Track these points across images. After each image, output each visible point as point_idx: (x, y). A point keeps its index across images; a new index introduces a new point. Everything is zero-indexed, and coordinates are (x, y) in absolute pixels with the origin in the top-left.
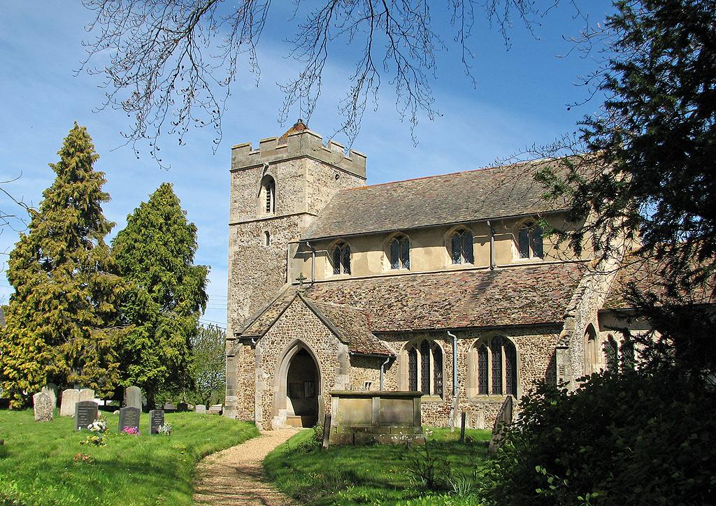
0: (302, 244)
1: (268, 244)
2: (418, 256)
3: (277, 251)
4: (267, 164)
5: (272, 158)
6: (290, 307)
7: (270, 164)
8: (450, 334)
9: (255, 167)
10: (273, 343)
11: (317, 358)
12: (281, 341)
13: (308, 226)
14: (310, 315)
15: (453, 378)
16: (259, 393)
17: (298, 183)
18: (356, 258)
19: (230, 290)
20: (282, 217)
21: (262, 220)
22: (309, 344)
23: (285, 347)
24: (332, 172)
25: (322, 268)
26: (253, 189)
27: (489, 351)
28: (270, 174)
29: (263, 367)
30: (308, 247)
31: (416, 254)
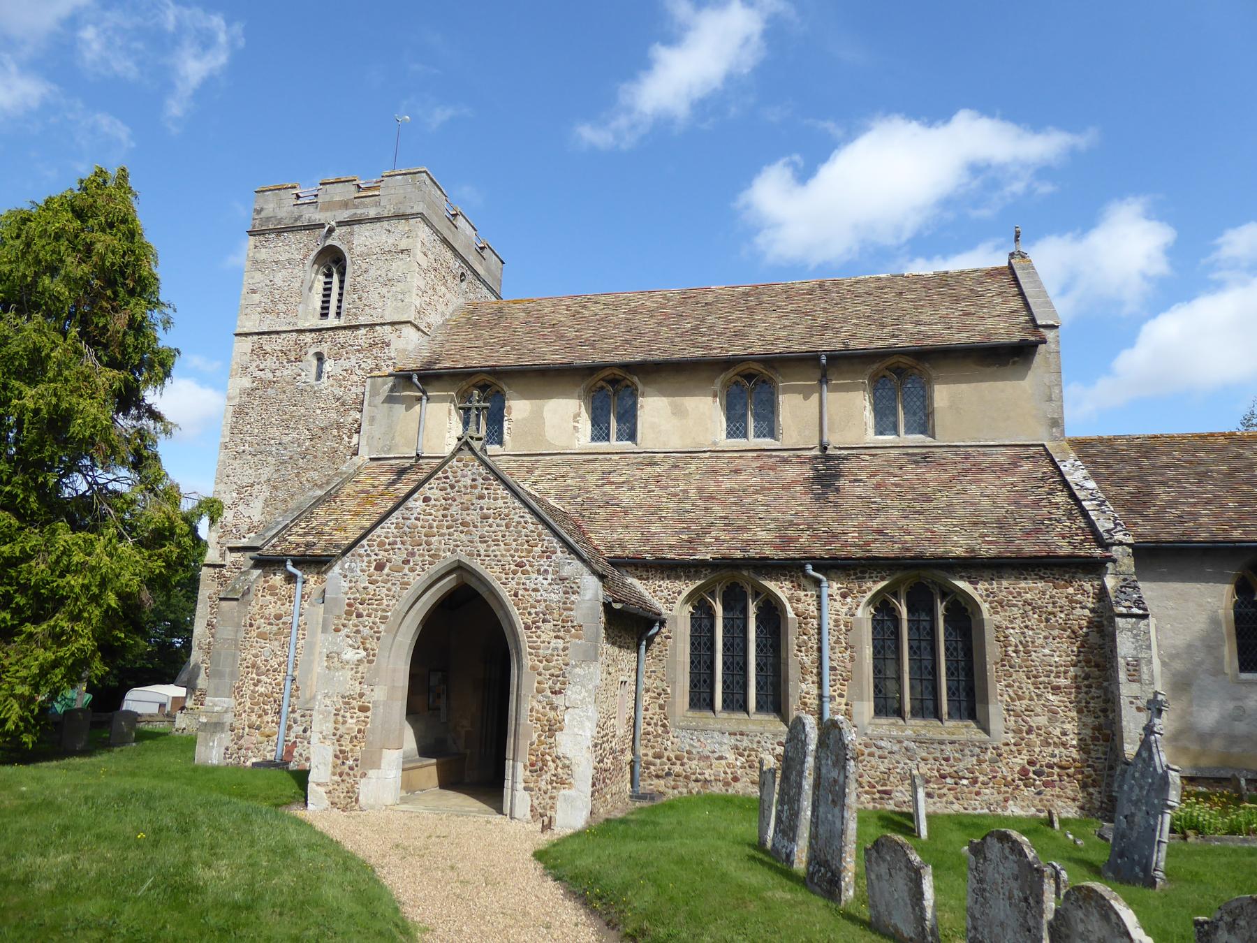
0: (403, 378)
1: (319, 377)
2: (655, 410)
3: (339, 392)
4: (333, 223)
5: (345, 215)
6: (440, 474)
7: (340, 224)
8: (813, 573)
9: (306, 228)
10: (380, 567)
11: (515, 612)
12: (406, 562)
13: (409, 348)
14: (500, 499)
15: (820, 674)
16: (328, 702)
17: (398, 266)
18: (518, 409)
19: (224, 465)
20: (357, 327)
21: (311, 331)
22: (491, 574)
23: (416, 580)
24: (456, 265)
25: (440, 425)
26: (295, 271)
27: (719, 609)
28: (336, 243)
29: (344, 631)
30: (421, 380)
31: (655, 410)
